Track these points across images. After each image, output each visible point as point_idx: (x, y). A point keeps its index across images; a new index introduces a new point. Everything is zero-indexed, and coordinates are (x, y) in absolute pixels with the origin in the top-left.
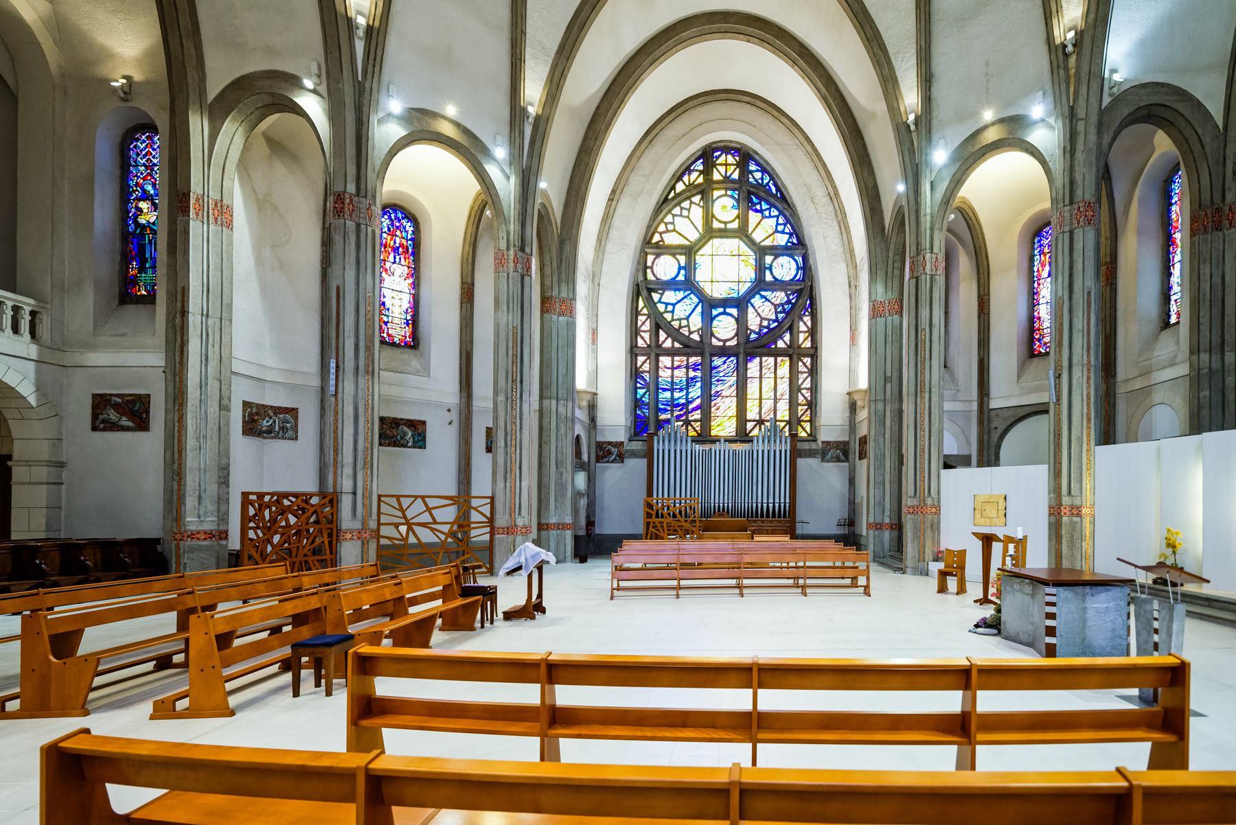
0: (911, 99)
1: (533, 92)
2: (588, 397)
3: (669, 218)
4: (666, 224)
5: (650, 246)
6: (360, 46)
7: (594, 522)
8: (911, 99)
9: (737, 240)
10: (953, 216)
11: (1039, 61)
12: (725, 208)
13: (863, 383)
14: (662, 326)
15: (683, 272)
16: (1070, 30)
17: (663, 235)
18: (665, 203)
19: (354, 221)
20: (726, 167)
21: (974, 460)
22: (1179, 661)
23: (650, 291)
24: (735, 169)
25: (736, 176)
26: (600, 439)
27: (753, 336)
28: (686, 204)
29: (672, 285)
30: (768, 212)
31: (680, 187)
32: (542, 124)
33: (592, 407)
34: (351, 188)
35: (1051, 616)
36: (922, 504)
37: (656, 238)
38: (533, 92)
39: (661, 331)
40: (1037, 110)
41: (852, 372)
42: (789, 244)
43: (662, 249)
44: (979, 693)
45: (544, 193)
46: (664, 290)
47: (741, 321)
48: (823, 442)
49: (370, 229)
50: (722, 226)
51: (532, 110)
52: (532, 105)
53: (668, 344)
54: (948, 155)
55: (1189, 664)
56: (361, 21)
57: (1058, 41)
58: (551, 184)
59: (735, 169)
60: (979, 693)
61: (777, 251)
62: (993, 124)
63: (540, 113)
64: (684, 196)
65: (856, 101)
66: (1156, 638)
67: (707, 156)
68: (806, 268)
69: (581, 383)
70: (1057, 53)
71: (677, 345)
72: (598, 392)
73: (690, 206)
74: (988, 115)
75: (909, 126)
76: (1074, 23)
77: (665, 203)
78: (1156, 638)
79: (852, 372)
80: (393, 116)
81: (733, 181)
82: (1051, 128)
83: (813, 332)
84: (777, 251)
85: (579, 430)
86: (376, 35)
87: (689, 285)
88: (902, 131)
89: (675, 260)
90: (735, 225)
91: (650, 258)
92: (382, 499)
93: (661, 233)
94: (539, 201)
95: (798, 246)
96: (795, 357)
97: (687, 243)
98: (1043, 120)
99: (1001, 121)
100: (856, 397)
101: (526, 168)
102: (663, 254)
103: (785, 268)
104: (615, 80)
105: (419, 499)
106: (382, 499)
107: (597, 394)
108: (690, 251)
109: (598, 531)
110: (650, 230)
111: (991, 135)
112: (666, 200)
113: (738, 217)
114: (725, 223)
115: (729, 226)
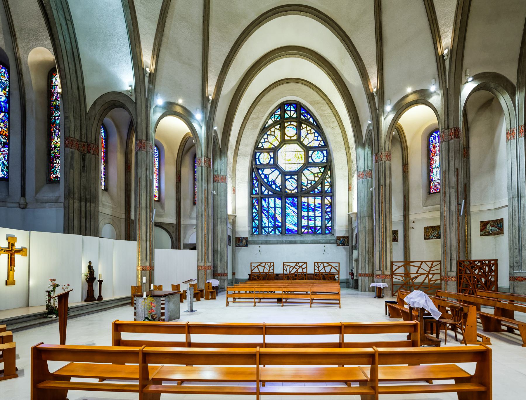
0: (374, 82)
1: (211, 89)
2: (232, 218)
3: (265, 136)
4: (264, 139)
5: (258, 149)
6: (147, 80)
7: (235, 273)
8: (374, 82)
9: (296, 145)
10: (394, 133)
11: (432, 68)
12: (291, 132)
13: (355, 210)
14: (263, 185)
15: (272, 160)
16: (445, 49)
17: (263, 144)
18: (264, 130)
19: (145, 151)
20: (291, 113)
21: (343, 328)
22: (486, 348)
23: (258, 169)
24: (294, 113)
25: (295, 116)
26: (237, 236)
27: (305, 188)
28: (273, 129)
29: (268, 166)
30: (317, 176)
31: (270, 122)
32: (215, 103)
33: (234, 223)
34: (144, 138)
35: (163, 308)
36: (383, 274)
37: (260, 145)
38: (211, 89)
39: (263, 187)
40: (433, 88)
41: (350, 205)
42: (320, 145)
43: (263, 150)
44: (344, 335)
45: (215, 131)
46: (264, 169)
47: (299, 181)
48: (337, 237)
49: (151, 153)
50: (289, 138)
51: (210, 98)
52: (211, 95)
53: (266, 192)
54: (391, 108)
55: (491, 350)
56: (148, 70)
57: (440, 54)
58: (218, 127)
59: (294, 113)
60: (344, 335)
61: (314, 149)
62: (411, 94)
63: (214, 98)
64: (299, 212)
65: (348, 82)
66: (163, 311)
67: (282, 107)
68: (329, 156)
69: (230, 212)
70: (440, 59)
71: (270, 193)
72: (236, 214)
73: (275, 130)
74: (409, 90)
75: (373, 94)
76: (447, 46)
77: (264, 130)
78: (163, 311)
79: (350, 205)
80: (159, 107)
81: (294, 118)
82: (438, 94)
83: (332, 185)
84: (314, 149)
85: (230, 233)
86: (152, 77)
87: (275, 166)
88: (370, 96)
89: (268, 155)
90: (295, 138)
91: (258, 154)
92: (394, 263)
93: (262, 143)
94: (213, 134)
95: (325, 147)
96: (324, 197)
97: (273, 146)
98: (435, 92)
99: (415, 92)
100: (352, 216)
101: (209, 119)
102: (263, 152)
103: (318, 157)
104: (244, 78)
105: (424, 263)
106: (394, 263)
107: (236, 216)
108: (284, 174)
109: (236, 277)
110: (257, 142)
111: (411, 98)
112: (264, 128)
113: (296, 134)
114: (291, 137)
115: (292, 138)
